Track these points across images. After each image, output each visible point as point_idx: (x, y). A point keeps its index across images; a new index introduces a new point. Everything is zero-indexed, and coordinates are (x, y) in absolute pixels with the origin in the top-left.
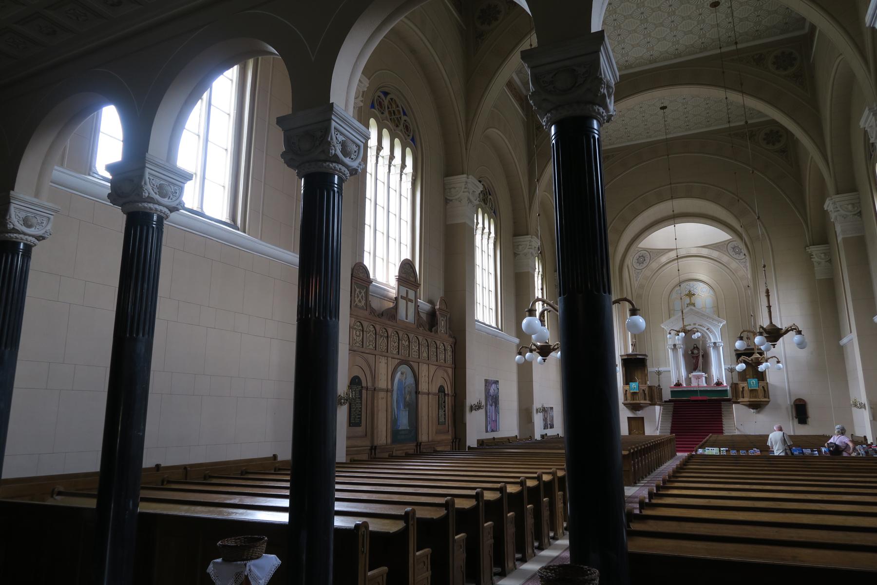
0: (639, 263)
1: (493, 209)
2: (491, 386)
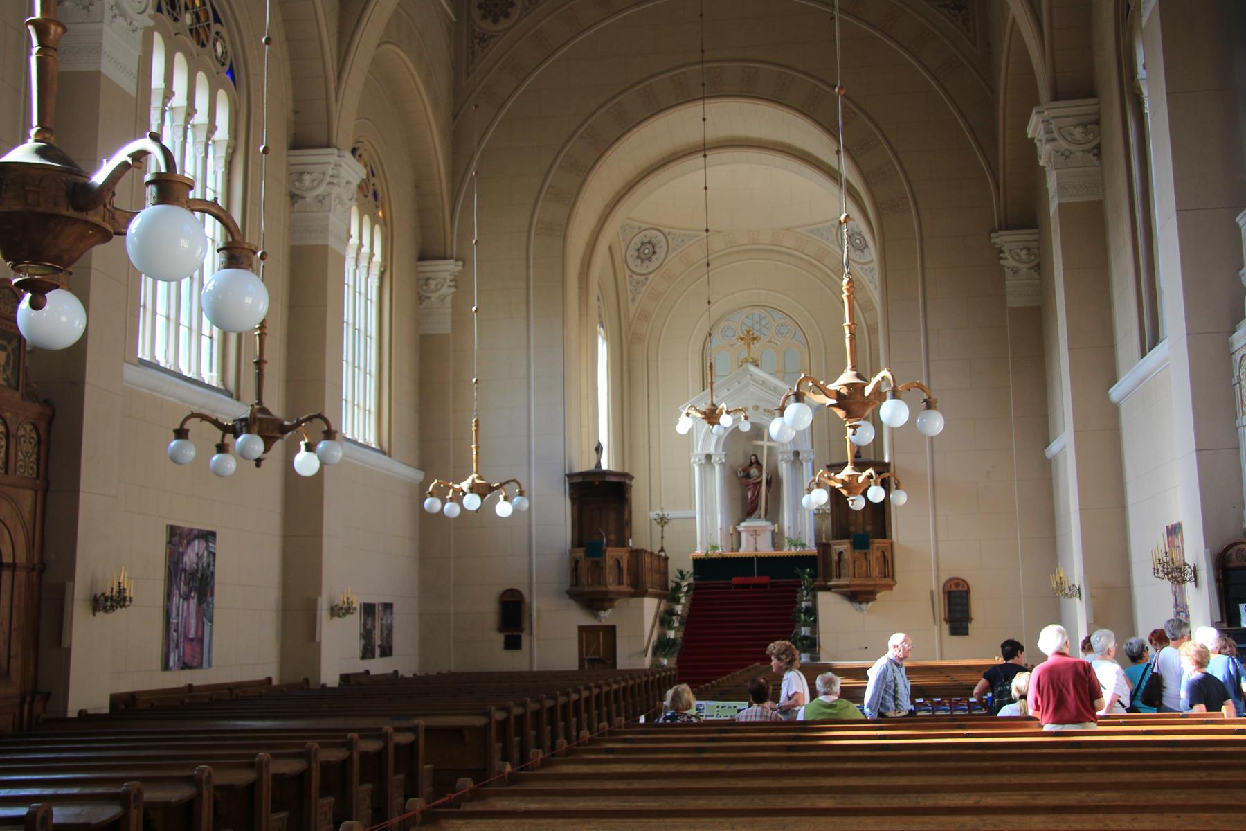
0: (643, 259)
1: (228, 63)
2: (189, 543)
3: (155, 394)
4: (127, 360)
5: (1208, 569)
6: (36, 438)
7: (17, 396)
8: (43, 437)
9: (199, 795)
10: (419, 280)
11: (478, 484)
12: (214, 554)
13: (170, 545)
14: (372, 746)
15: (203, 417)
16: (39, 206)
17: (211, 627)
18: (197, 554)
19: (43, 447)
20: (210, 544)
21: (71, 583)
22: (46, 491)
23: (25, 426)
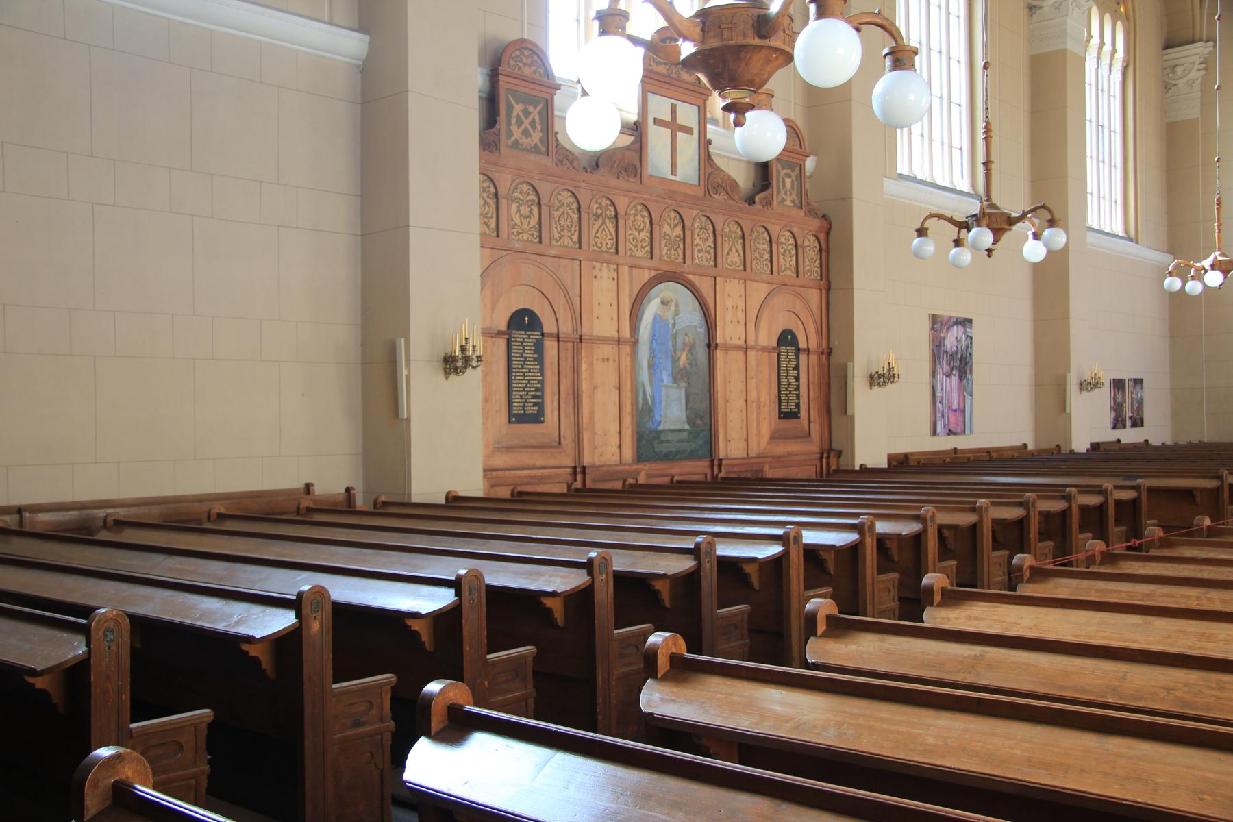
2: (948, 329)
3: (914, 203)
4: (888, 175)
5: (964, 18)
6: (818, 248)
7: (802, 213)
8: (824, 246)
9: (925, 530)
10: (1165, 68)
11: (1220, 261)
12: (971, 338)
13: (933, 331)
14: (1093, 500)
15: (940, 217)
16: (732, 40)
17: (971, 399)
18: (957, 338)
19: (824, 254)
20: (967, 329)
21: (852, 363)
22: (828, 289)
23: (758, 229)
